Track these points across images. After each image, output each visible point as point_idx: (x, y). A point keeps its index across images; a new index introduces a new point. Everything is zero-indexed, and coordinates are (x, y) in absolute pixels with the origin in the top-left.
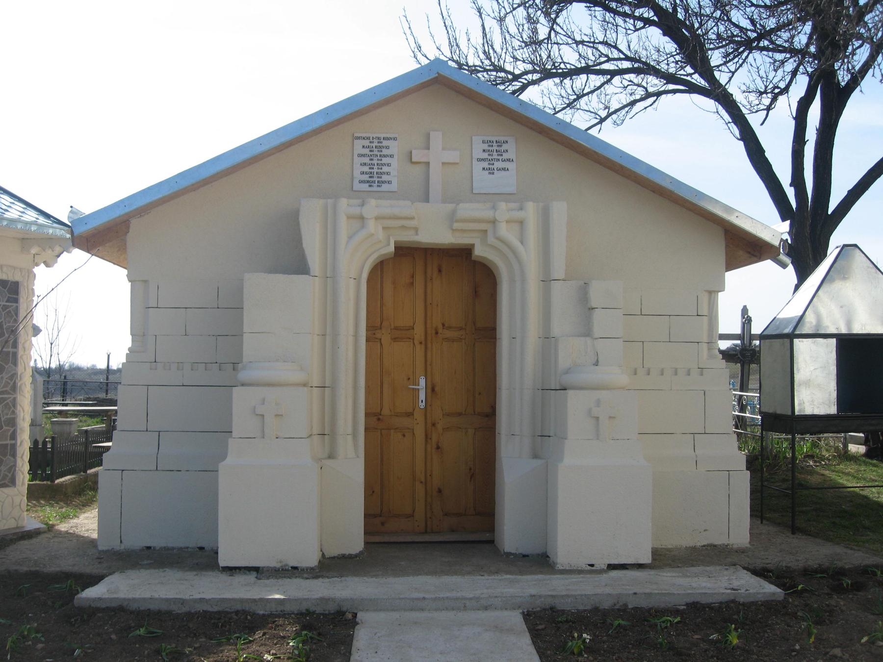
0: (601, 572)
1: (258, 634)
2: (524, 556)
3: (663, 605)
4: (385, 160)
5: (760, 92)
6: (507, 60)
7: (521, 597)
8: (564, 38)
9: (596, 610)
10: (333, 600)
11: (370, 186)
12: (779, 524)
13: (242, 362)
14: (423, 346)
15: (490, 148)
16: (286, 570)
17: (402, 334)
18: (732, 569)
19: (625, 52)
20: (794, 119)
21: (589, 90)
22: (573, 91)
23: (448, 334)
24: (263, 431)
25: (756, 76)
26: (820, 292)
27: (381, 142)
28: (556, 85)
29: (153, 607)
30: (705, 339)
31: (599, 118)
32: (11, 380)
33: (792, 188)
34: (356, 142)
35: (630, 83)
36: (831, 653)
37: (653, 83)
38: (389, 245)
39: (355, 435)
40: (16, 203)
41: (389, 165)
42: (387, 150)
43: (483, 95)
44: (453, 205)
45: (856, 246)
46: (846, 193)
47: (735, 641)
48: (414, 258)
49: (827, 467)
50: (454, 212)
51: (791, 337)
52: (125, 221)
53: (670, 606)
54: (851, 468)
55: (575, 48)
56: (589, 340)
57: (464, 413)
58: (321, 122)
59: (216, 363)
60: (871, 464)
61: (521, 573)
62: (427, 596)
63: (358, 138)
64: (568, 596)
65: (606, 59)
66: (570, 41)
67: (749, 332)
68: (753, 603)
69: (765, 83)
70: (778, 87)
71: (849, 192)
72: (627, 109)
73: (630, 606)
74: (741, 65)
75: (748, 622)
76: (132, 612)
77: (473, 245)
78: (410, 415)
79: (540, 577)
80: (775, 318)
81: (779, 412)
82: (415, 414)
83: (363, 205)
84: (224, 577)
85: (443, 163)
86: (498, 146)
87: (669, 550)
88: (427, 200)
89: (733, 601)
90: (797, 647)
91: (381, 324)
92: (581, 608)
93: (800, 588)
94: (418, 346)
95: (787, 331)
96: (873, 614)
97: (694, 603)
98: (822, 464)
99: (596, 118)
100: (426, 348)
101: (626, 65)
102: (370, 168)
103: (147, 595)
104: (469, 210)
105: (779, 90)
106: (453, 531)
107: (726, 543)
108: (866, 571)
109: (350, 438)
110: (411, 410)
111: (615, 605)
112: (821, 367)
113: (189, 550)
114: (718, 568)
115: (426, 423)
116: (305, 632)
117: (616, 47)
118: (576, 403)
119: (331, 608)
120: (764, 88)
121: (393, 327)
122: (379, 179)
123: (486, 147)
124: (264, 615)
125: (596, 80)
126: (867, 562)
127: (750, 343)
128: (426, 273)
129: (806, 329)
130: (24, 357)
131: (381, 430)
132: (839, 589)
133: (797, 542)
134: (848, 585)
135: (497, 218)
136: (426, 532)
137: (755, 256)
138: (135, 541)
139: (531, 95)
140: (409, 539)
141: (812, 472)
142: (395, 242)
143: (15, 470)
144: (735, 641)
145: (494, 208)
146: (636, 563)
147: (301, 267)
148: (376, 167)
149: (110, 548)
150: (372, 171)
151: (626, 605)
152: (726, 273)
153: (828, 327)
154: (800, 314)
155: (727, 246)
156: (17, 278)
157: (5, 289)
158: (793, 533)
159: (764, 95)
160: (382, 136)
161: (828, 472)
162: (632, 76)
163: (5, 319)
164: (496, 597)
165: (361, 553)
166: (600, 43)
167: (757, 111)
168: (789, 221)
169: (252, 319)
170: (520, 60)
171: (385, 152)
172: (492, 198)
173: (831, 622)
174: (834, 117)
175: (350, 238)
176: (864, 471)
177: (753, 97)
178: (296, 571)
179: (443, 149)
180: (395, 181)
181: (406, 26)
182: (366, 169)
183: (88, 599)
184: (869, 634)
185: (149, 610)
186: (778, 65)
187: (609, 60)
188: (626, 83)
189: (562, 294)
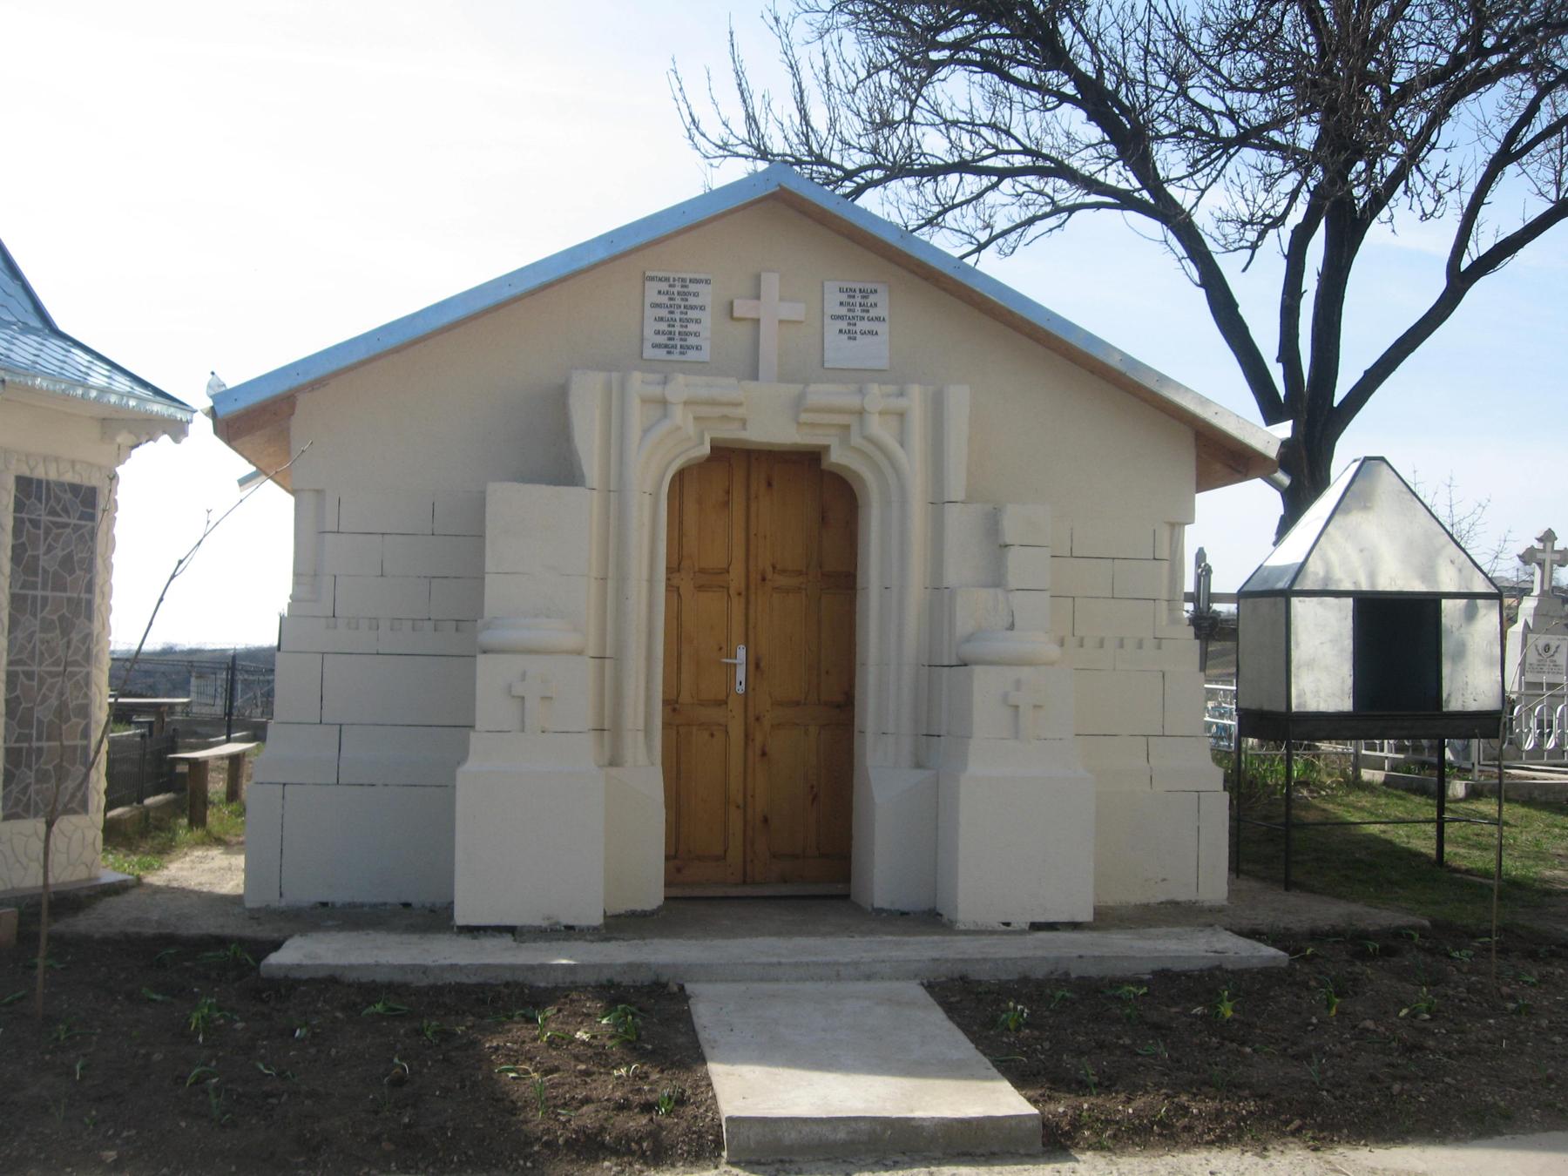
0: (1022, 932)
1: (551, 1011)
2: (903, 914)
3: (1119, 974)
4: (692, 314)
5: (1242, 221)
6: (835, 147)
7: (919, 961)
8: (928, 115)
9: (1025, 980)
10: (648, 966)
11: (669, 353)
12: (1263, 879)
13: (482, 617)
14: (743, 600)
15: (851, 300)
16: (556, 931)
17: (711, 580)
18: (1208, 931)
19: (1022, 140)
20: (1286, 257)
21: (963, 199)
22: (937, 198)
23: (782, 581)
24: (523, 722)
25: (1237, 198)
26: (1330, 528)
27: (686, 286)
28: (909, 188)
29: (381, 977)
30: (1164, 595)
31: (976, 242)
32: (84, 644)
33: (1280, 366)
34: (648, 284)
35: (1027, 189)
36: (1361, 1026)
37: (1067, 193)
38: (702, 443)
39: (647, 731)
40: (95, 362)
41: (698, 321)
42: (695, 298)
43: (845, 220)
44: (801, 386)
45: (1382, 459)
46: (1362, 375)
47: (1229, 1014)
48: (730, 465)
49: (1331, 798)
50: (802, 397)
51: (1287, 594)
52: (289, 397)
53: (1129, 974)
54: (1366, 801)
55: (944, 131)
56: (999, 591)
57: (803, 701)
58: (601, 254)
59: (430, 619)
60: (1396, 796)
61: (905, 933)
62: (783, 960)
63: (652, 279)
64: (985, 960)
65: (993, 151)
66: (938, 120)
67: (1206, 592)
68: (1247, 971)
69: (1251, 208)
70: (1269, 216)
71: (1366, 372)
72: (1020, 230)
73: (1073, 976)
74: (1214, 180)
75: (1241, 994)
76: (350, 985)
77: (827, 448)
78: (723, 703)
79: (936, 938)
80: (1261, 566)
81: (1266, 707)
82: (729, 703)
83: (665, 382)
84: (465, 941)
85: (781, 322)
86: (863, 297)
87: (1111, 908)
88: (755, 376)
89: (1219, 968)
90: (1314, 1020)
91: (679, 564)
92: (1004, 977)
93: (1309, 952)
94: (735, 599)
95: (1281, 585)
96: (1414, 985)
97: (1163, 970)
98: (1321, 796)
99: (971, 243)
100: (748, 602)
101: (1019, 161)
102: (669, 326)
103: (370, 960)
104: (822, 393)
105: (1271, 220)
106: (784, 880)
107: (1193, 900)
108: (1397, 933)
109: (641, 736)
110: (722, 696)
111: (1052, 973)
112: (1331, 641)
113: (366, 909)
114: (1188, 929)
115: (746, 717)
116: (623, 1006)
117: (1008, 133)
118: (986, 685)
119: (645, 978)
120: (1247, 214)
121: (697, 569)
122: (683, 343)
123: (844, 297)
124: (546, 989)
125: (972, 183)
126: (1400, 922)
127: (1209, 608)
128: (748, 487)
129: (1308, 584)
130: (103, 608)
131: (678, 726)
132: (1362, 955)
133: (1294, 899)
134: (1375, 949)
135: (867, 408)
136: (744, 882)
137: (1239, 472)
138: (305, 892)
139: (870, 201)
140: (719, 892)
141: (1308, 806)
142: (712, 440)
143: (87, 788)
144: (1229, 1014)
145: (861, 392)
146: (1071, 920)
147: (565, 473)
148: (678, 324)
149: (264, 905)
150: (672, 329)
151: (1067, 974)
152: (1197, 495)
153: (1340, 581)
154: (1301, 560)
155: (1198, 457)
156: (95, 480)
157: (77, 497)
158: (1287, 889)
159: (1249, 227)
160: (688, 276)
161: (1331, 806)
162: (1032, 180)
163: (76, 546)
164: (883, 961)
165: (660, 909)
166: (984, 125)
167: (1235, 250)
168: (1290, 422)
169: (498, 552)
170: (854, 147)
171: (692, 301)
172: (860, 377)
173: (1356, 993)
174: (1345, 255)
175: (646, 431)
176: (1386, 804)
177: (1230, 229)
178: (572, 932)
179: (782, 299)
180: (706, 346)
181: (676, 86)
182: (663, 326)
183: (280, 967)
184: (1408, 1007)
185: (373, 981)
186: (1270, 180)
187: (998, 152)
188: (1020, 189)
189: (961, 522)
